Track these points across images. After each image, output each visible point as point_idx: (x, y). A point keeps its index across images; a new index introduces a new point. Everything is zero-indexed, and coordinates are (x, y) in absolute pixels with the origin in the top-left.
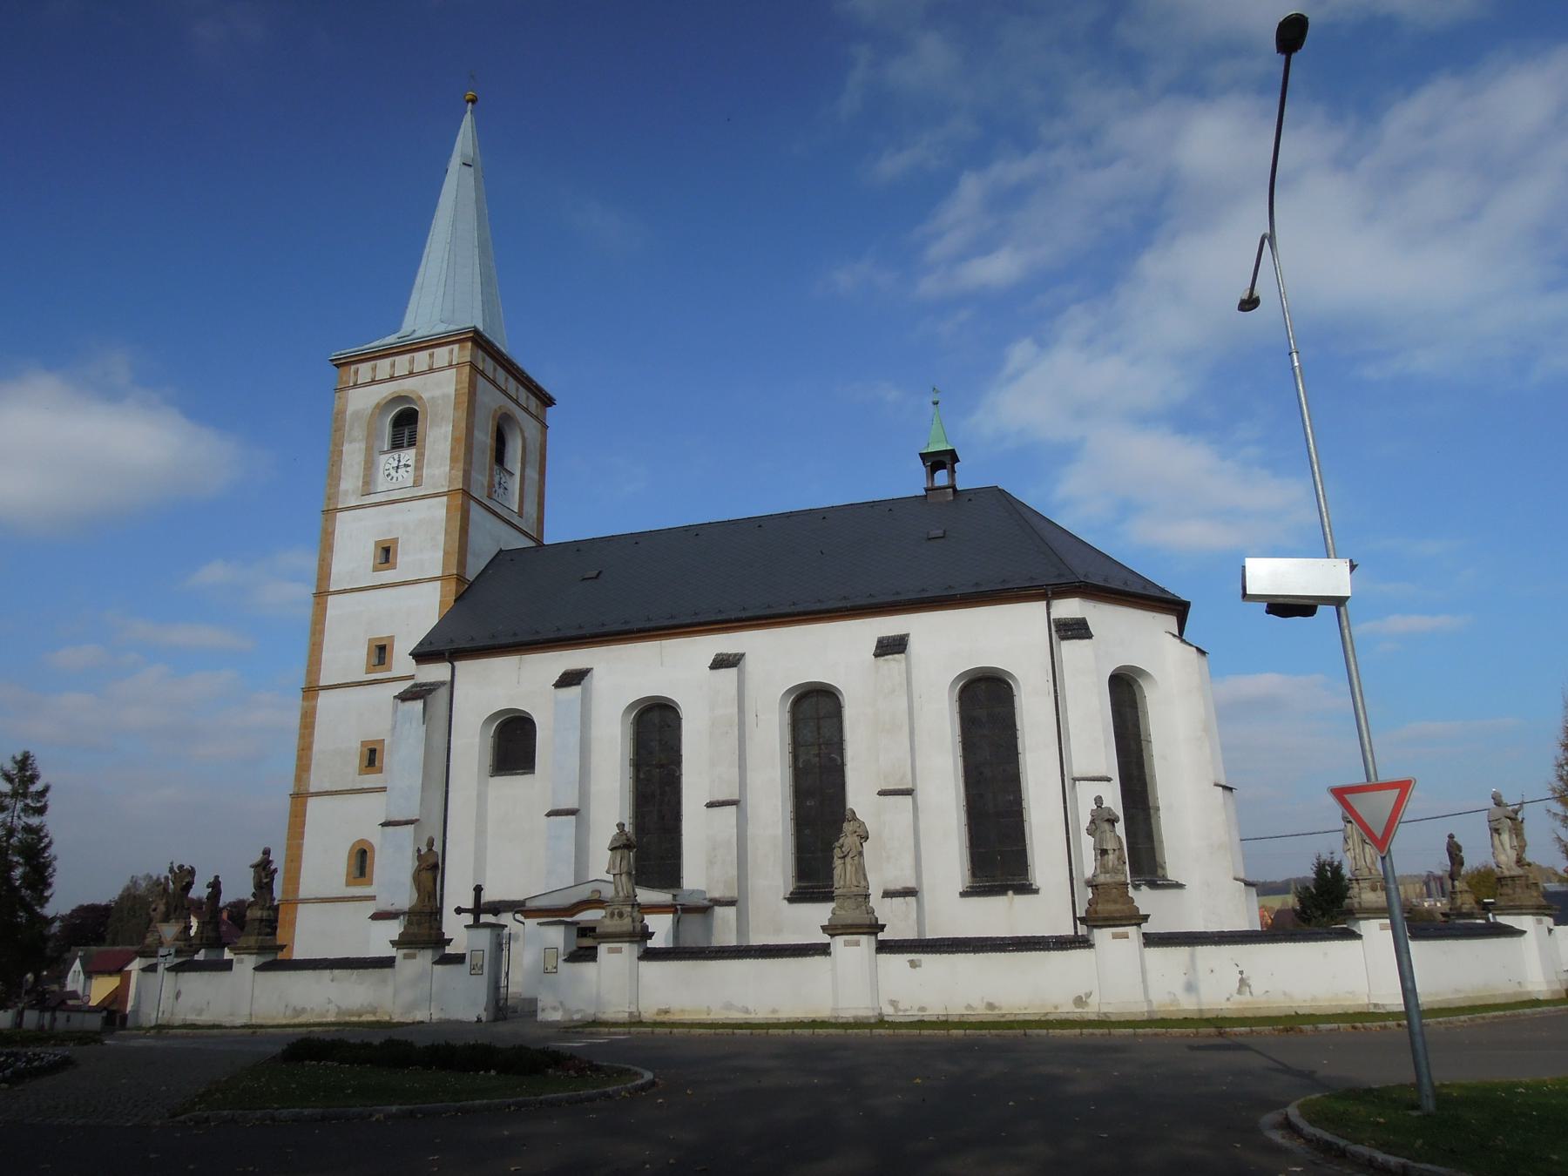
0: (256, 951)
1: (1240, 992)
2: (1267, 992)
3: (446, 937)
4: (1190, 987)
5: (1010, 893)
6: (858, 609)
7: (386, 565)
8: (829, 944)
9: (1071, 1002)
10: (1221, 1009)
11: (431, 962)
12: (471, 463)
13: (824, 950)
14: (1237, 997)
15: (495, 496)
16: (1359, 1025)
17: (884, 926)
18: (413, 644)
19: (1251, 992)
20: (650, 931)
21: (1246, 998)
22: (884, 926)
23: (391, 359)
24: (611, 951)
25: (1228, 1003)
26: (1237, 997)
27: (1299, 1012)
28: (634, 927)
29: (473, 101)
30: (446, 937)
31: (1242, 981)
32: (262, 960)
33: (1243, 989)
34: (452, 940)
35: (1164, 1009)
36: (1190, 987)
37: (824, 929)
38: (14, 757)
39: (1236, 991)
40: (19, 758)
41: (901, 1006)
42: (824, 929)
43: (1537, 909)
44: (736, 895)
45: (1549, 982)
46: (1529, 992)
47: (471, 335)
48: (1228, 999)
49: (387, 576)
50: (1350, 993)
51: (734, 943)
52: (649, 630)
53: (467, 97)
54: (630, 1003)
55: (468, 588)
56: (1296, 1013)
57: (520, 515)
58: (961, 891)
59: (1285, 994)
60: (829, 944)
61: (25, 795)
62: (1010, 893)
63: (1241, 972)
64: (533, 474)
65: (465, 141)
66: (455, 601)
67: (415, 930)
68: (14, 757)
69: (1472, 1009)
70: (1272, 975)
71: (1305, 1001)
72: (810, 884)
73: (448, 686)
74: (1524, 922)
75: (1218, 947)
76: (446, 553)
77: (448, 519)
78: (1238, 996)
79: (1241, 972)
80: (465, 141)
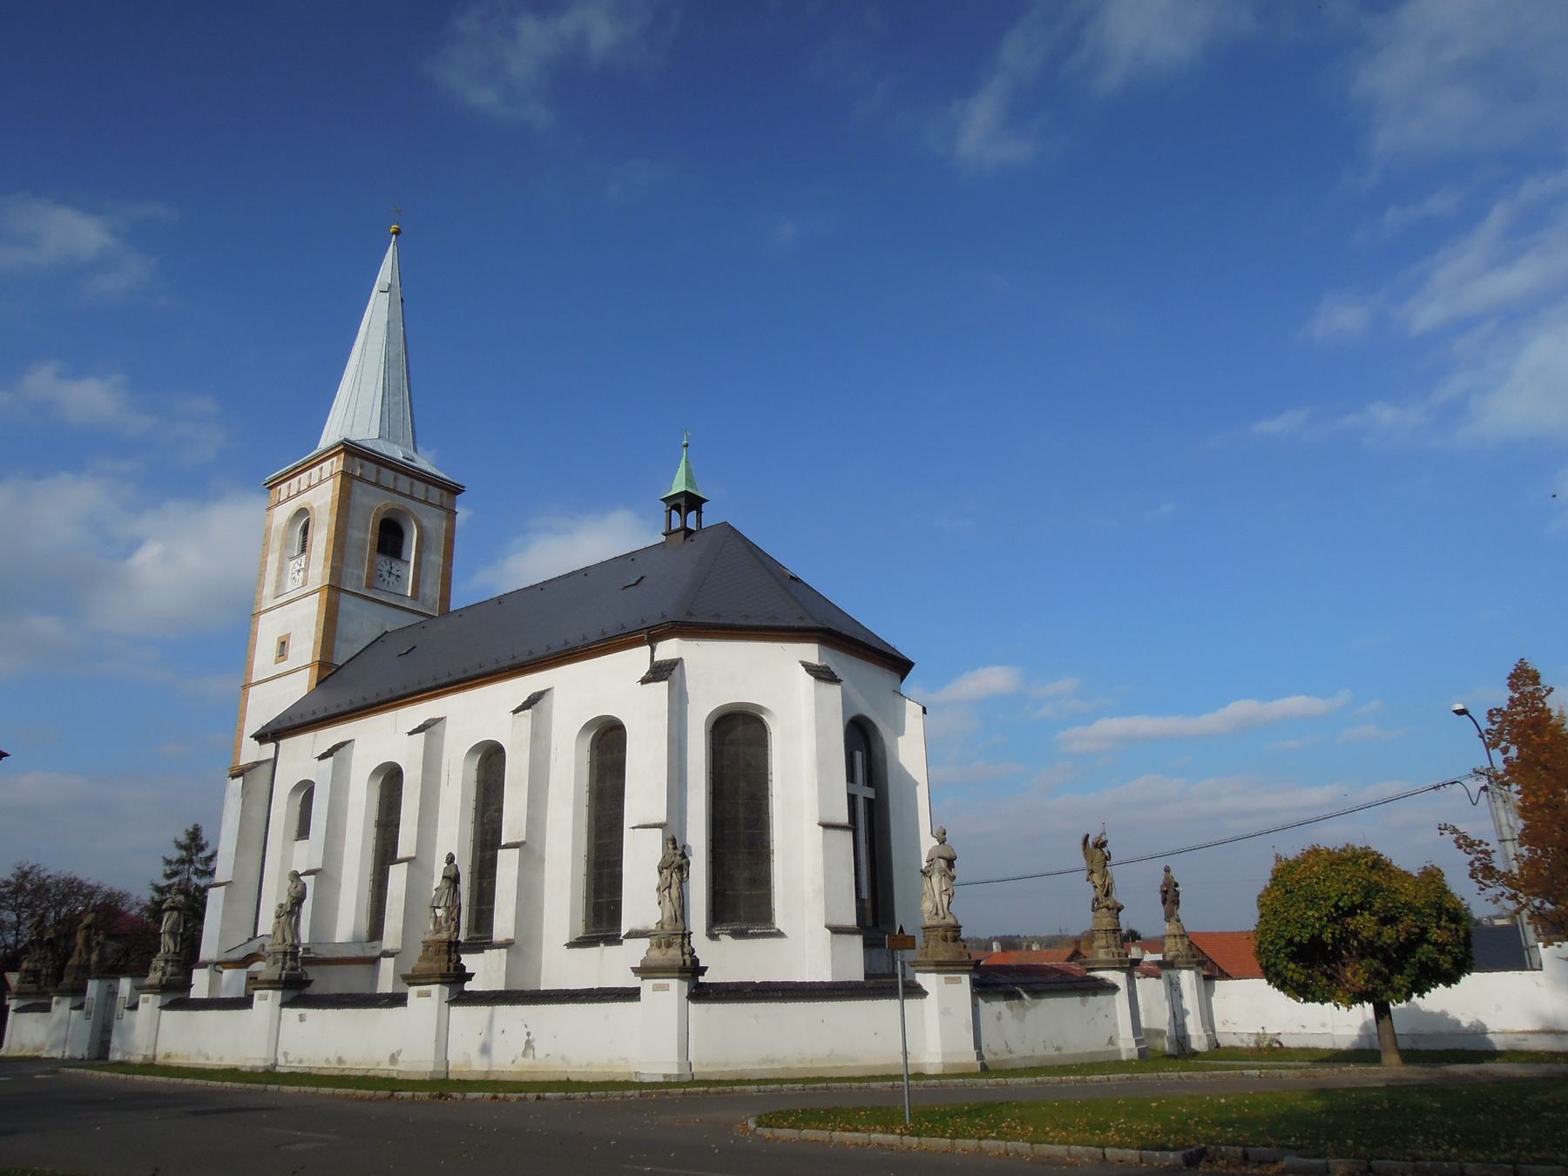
0: (439, 980)
1: (524, 1055)
2: (548, 1055)
3: (467, 971)
4: (485, 1049)
5: (602, 945)
6: (517, 668)
7: (282, 658)
8: (639, 989)
9: (388, 1059)
10: (503, 1072)
11: (69, 1007)
12: (342, 561)
13: (631, 995)
14: (521, 1060)
15: (378, 585)
16: (501, 1095)
17: (705, 969)
18: (256, 728)
19: (534, 1056)
20: (701, 965)
21: (529, 1061)
22: (705, 969)
23: (297, 478)
24: (420, 995)
25: (513, 1065)
26: (521, 1060)
27: (571, 1078)
28: (684, 960)
29: (397, 233)
30: (467, 971)
31: (528, 1043)
32: (23, 1003)
33: (528, 1052)
34: (473, 974)
35: (457, 1069)
36: (485, 1049)
37: (635, 970)
38: (187, 830)
39: (521, 1054)
40: (191, 830)
41: (290, 1059)
42: (635, 970)
43: (936, 965)
44: (400, 947)
45: (944, 1055)
46: (922, 1065)
47: (342, 447)
48: (513, 1062)
49: (284, 666)
50: (622, 1059)
51: (205, 996)
52: (387, 701)
53: (392, 230)
54: (148, 1047)
55: (335, 671)
56: (568, 1078)
57: (415, 596)
58: (568, 941)
59: (563, 1058)
60: (639, 989)
61: (191, 862)
62: (602, 945)
63: (528, 1034)
64: (435, 559)
65: (387, 272)
66: (317, 684)
67: (656, 954)
68: (187, 830)
69: (806, 1080)
70: (555, 1036)
71: (581, 1066)
72: (479, 935)
73: (271, 764)
74: (927, 980)
75: (512, 1006)
76: (315, 643)
77: (319, 612)
78: (523, 1059)
79: (528, 1034)
80: (387, 272)
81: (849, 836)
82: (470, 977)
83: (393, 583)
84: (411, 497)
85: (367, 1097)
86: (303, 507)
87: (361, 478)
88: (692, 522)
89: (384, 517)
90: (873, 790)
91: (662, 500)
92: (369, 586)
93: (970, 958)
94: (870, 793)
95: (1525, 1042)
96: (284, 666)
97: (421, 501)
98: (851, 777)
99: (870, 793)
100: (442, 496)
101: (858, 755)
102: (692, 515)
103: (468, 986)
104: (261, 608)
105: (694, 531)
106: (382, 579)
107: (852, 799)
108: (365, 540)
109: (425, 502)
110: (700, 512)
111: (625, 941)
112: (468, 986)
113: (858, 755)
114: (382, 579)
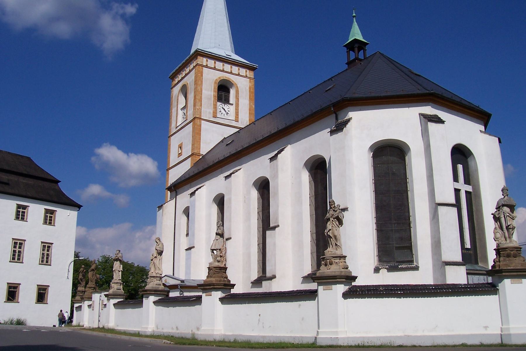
8: (202, 296)
17: (356, 277)
60: (202, 296)
81: (455, 210)
82: (233, 286)
83: (224, 115)
84: (231, 73)
85: (166, 343)
86: (184, 84)
87: (206, 66)
88: (361, 55)
89: (220, 84)
90: (471, 186)
91: (344, 46)
92: (215, 116)
93: (499, 267)
94: (469, 188)
95: (228, 173)
96: (182, 158)
97: (236, 75)
98: (456, 179)
99: (469, 188)
100: (246, 71)
101: (460, 167)
102: (361, 52)
103: (233, 291)
104: (171, 133)
105: (363, 60)
106: (221, 113)
107: (457, 191)
108: (211, 95)
109: (238, 75)
110: (365, 51)
111: (226, 266)
112: (233, 291)
113: (460, 167)
114: (221, 113)
